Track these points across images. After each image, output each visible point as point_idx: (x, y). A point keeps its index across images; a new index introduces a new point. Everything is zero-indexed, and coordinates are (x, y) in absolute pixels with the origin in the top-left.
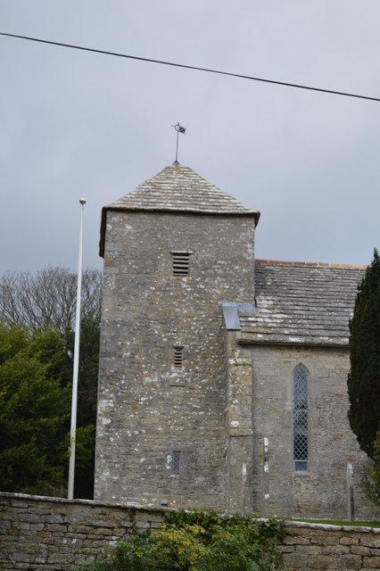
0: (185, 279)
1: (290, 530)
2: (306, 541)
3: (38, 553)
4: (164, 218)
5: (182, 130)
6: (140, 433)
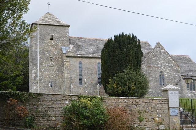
0: (52, 41)
1: (104, 98)
2: (108, 100)
3: (50, 105)
6: (43, 78)
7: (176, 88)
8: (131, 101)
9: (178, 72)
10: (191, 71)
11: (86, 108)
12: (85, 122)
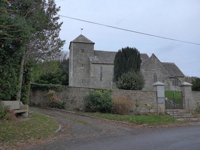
4: (80, 44)
5: (82, 29)
7: (162, 84)
8: (131, 93)
9: (166, 74)
10: (175, 73)
11: (99, 97)
12: (98, 106)
